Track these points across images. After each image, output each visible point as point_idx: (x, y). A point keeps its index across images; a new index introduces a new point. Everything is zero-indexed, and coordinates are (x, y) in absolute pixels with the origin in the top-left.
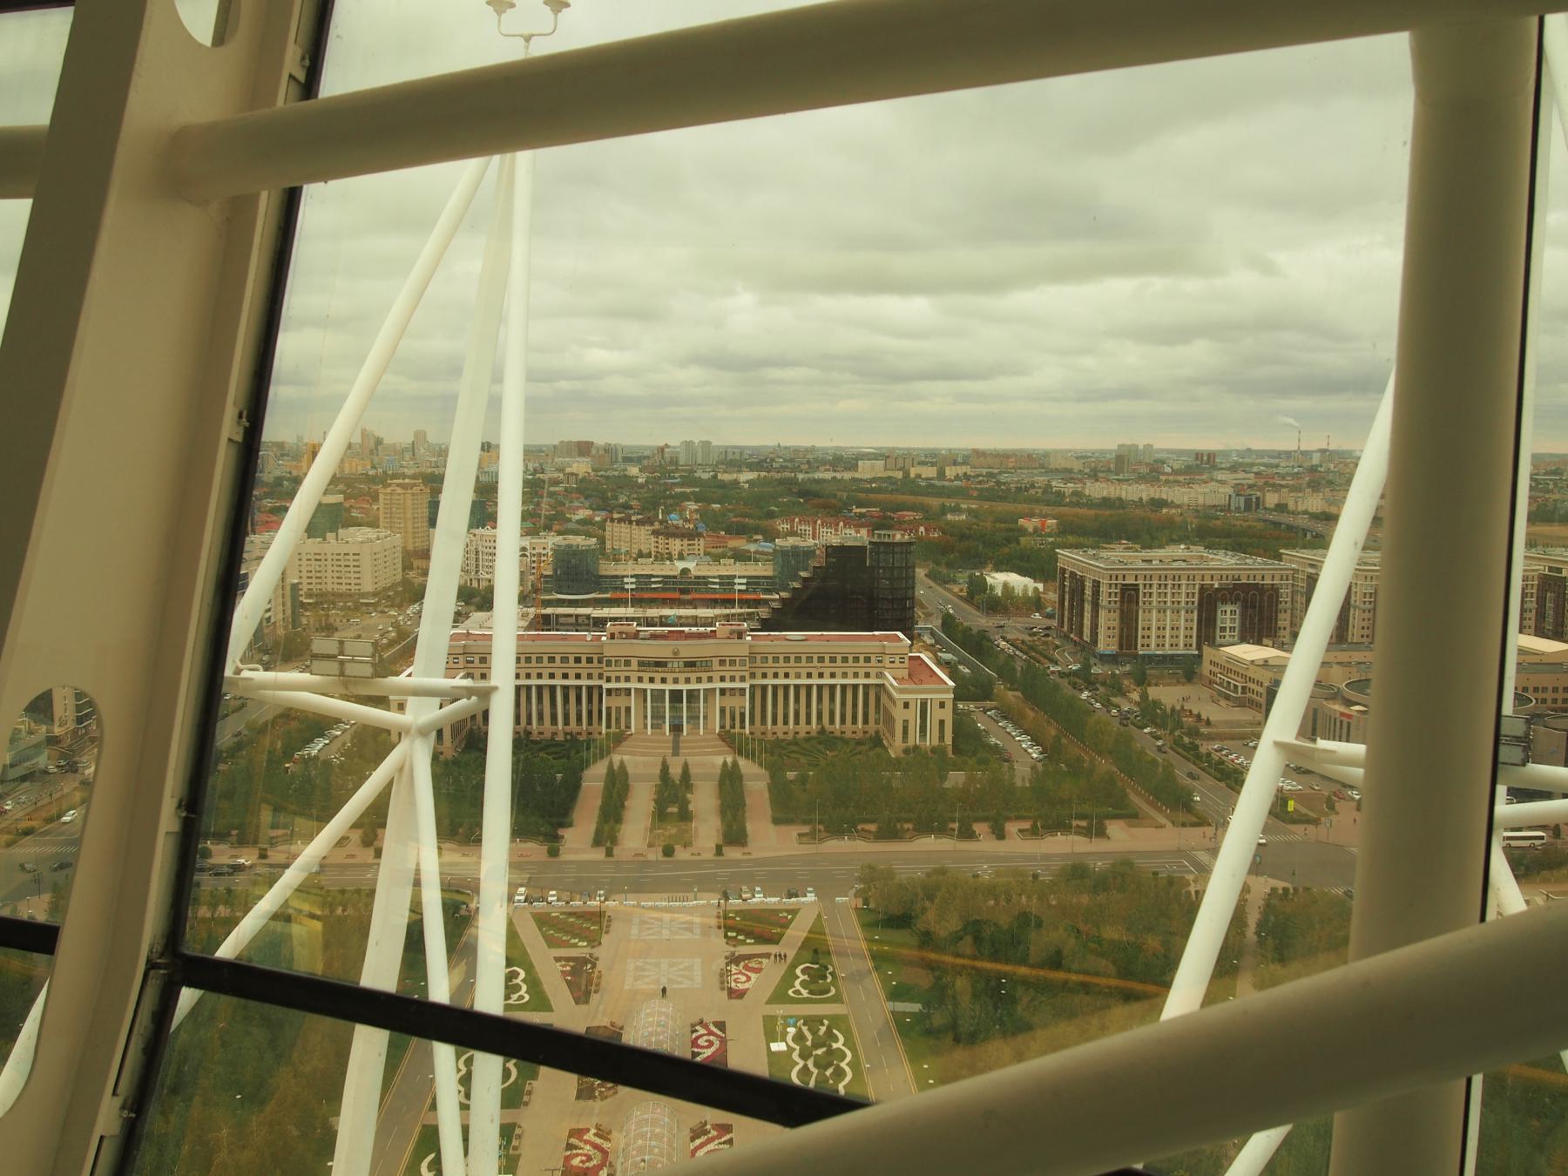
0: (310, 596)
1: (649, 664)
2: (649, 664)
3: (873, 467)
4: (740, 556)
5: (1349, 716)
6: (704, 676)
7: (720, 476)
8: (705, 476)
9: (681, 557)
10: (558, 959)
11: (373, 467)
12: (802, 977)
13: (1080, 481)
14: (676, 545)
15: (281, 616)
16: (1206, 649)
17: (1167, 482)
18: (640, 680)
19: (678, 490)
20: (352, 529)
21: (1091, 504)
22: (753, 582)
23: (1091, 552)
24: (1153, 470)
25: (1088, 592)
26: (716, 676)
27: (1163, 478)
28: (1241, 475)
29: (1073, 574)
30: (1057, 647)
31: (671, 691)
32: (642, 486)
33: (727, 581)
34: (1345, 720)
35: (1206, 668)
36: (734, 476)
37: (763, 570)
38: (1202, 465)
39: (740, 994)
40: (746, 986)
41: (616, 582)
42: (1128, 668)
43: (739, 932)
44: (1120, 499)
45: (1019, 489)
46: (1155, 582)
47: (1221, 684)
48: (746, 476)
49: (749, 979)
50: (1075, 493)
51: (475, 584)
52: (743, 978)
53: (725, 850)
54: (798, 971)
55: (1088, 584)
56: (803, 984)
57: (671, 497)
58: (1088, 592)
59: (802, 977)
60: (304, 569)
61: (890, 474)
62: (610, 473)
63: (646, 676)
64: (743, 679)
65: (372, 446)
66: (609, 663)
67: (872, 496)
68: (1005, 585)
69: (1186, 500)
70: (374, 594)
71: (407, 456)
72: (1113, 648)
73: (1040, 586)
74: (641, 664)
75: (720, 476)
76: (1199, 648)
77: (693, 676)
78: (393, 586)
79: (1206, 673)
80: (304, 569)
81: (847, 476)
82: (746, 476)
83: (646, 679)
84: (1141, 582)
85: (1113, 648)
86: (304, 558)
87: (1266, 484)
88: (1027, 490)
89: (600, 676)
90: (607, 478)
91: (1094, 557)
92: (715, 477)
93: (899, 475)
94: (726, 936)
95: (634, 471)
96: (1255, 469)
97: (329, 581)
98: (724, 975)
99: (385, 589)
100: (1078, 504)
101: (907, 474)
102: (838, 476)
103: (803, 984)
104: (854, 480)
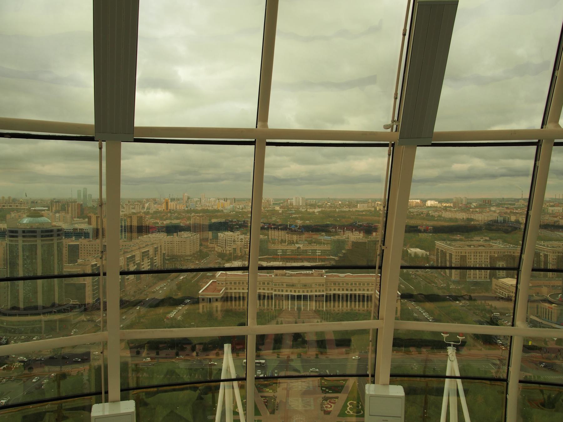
0: (168, 256)
1: (290, 285)
2: (290, 285)
3: (363, 206)
4: (319, 243)
5: (552, 308)
6: (309, 290)
7: (308, 210)
8: (303, 210)
9: (297, 243)
10: (262, 397)
11: (187, 207)
12: (350, 406)
13: (440, 211)
14: (295, 237)
15: (160, 264)
16: (493, 279)
17: (473, 211)
18: (287, 291)
19: (294, 216)
20: (183, 232)
21: (445, 220)
22: (323, 252)
23: (448, 242)
24: (466, 208)
25: (448, 258)
26: (314, 290)
27: (471, 210)
28: (501, 208)
29: (442, 251)
30: (436, 277)
31: (304, 296)
32: (280, 214)
33: (314, 251)
34: (550, 310)
35: (494, 286)
36: (313, 210)
37: (327, 247)
38: (486, 204)
39: (327, 413)
40: (330, 409)
41: (275, 252)
42: (463, 286)
43: (327, 388)
44: (456, 218)
45: (417, 215)
46: (473, 254)
47: (500, 293)
48: (317, 210)
49: (331, 406)
50: (439, 216)
51: (225, 252)
52: (329, 406)
53: (320, 356)
54: (348, 404)
55: (448, 255)
56: (350, 409)
57: (292, 218)
58: (448, 258)
59: (350, 406)
60: (167, 247)
61: (370, 208)
62: (269, 209)
63: (289, 290)
64: (323, 291)
65: (186, 199)
66: (276, 285)
67: (363, 217)
68: (415, 253)
69: (480, 218)
70: (190, 256)
71: (198, 203)
72: (458, 279)
73: (428, 253)
74: (287, 285)
75: (308, 210)
76: (490, 278)
77: (305, 290)
78: (197, 252)
79: (493, 288)
80: (167, 247)
81: (354, 209)
82: (317, 210)
83: (289, 291)
84: (467, 254)
85: (458, 279)
86: (166, 243)
87: (511, 212)
88: (420, 215)
89: (272, 289)
90: (268, 211)
91: (450, 245)
92: (307, 210)
93: (373, 209)
94: (322, 389)
95: (277, 208)
96: (506, 206)
97: (175, 251)
98: (322, 404)
99: (194, 254)
100: (440, 220)
101: (376, 209)
102: (351, 210)
103: (350, 409)
104: (356, 211)
